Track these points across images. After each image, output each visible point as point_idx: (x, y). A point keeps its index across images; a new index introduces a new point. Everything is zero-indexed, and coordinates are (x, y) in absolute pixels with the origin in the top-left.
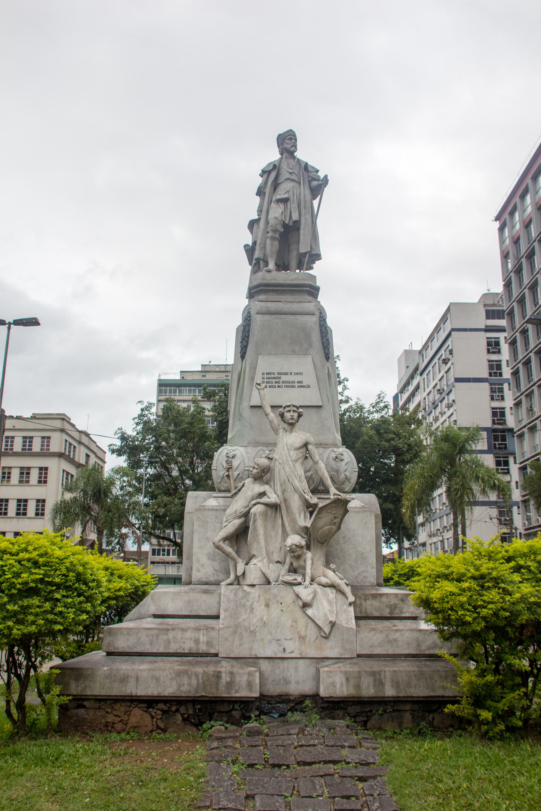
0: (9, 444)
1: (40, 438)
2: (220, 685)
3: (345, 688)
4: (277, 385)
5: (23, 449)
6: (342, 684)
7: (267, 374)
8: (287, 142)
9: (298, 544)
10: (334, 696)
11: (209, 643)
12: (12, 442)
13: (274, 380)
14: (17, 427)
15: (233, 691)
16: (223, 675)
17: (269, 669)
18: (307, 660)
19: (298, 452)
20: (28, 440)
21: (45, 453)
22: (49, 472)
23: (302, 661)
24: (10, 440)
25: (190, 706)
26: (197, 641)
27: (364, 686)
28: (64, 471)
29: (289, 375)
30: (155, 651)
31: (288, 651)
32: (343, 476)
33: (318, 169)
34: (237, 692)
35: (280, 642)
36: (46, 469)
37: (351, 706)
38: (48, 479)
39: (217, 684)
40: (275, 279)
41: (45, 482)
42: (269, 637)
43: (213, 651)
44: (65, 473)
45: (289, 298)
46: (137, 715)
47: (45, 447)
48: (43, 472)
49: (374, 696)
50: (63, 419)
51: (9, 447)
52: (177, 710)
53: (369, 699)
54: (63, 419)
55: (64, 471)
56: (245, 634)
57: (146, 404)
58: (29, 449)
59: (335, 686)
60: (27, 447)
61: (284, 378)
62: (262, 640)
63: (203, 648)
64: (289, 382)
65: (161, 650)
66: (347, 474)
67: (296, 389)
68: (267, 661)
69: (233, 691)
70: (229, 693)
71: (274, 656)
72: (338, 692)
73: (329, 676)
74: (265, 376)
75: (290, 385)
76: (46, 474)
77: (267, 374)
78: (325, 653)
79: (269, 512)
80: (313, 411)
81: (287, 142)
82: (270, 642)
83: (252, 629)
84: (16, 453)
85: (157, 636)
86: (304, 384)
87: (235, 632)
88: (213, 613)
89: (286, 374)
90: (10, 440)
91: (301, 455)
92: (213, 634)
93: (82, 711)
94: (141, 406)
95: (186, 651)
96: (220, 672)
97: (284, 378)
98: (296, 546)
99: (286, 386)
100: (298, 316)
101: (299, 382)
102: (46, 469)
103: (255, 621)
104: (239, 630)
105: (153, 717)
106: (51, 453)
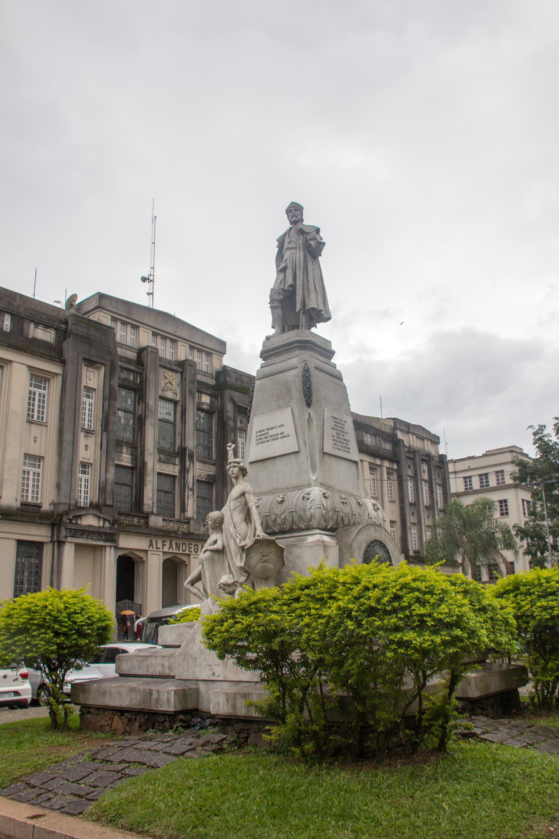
0: (468, 483)
1: (462, 479)
2: (152, 701)
3: (226, 707)
4: (266, 440)
5: (481, 487)
6: (224, 703)
7: (260, 432)
8: (295, 212)
9: (225, 583)
10: (219, 713)
11: (170, 668)
12: (470, 481)
13: (264, 436)
14: (472, 467)
15: (159, 706)
16: (154, 692)
17: (205, 690)
18: (229, 683)
19: (235, 502)
20: (484, 477)
21: (501, 487)
22: (509, 503)
23: (225, 683)
24: (468, 480)
25: (142, 715)
26: (163, 666)
27: (238, 706)
28: (523, 500)
29: (274, 430)
30: (141, 673)
31: (216, 674)
32: (308, 514)
33: (318, 226)
34: (161, 706)
35: (211, 667)
36: (506, 501)
37: (237, 723)
38: (509, 511)
39: (151, 700)
40: (273, 344)
41: (507, 514)
42: (205, 663)
43: (172, 674)
44: (525, 502)
45: (277, 359)
46: (118, 722)
47: (501, 481)
48: (503, 504)
49: (245, 715)
50: (512, 451)
51: (469, 487)
52: (135, 719)
53: (244, 719)
54: (512, 451)
55: (523, 500)
56: (191, 660)
57: (537, 428)
58: (487, 486)
59: (219, 705)
60: (485, 484)
61: (271, 432)
62: (200, 665)
63: (167, 672)
64: (274, 435)
65: (144, 673)
66: (312, 511)
67: (280, 440)
68: (203, 683)
69: (159, 706)
70: (157, 707)
71: (207, 679)
72: (221, 710)
73: (216, 697)
74: (258, 434)
75: (275, 438)
76: (506, 505)
77: (260, 432)
78: (240, 677)
79: (216, 556)
80: (293, 457)
81: (295, 212)
82: (205, 667)
83: (194, 656)
84: (475, 491)
85: (142, 661)
86: (285, 434)
87: (184, 659)
88: (177, 643)
89: (272, 428)
90: (468, 480)
91: (238, 504)
92: (172, 660)
93: (89, 716)
94: (532, 431)
95: (158, 674)
96: (152, 690)
97: (271, 432)
98: (224, 584)
99: (272, 440)
100: (286, 373)
101: (281, 434)
102: (506, 501)
103: (196, 649)
104: (187, 658)
105: (123, 723)
106: (506, 485)
